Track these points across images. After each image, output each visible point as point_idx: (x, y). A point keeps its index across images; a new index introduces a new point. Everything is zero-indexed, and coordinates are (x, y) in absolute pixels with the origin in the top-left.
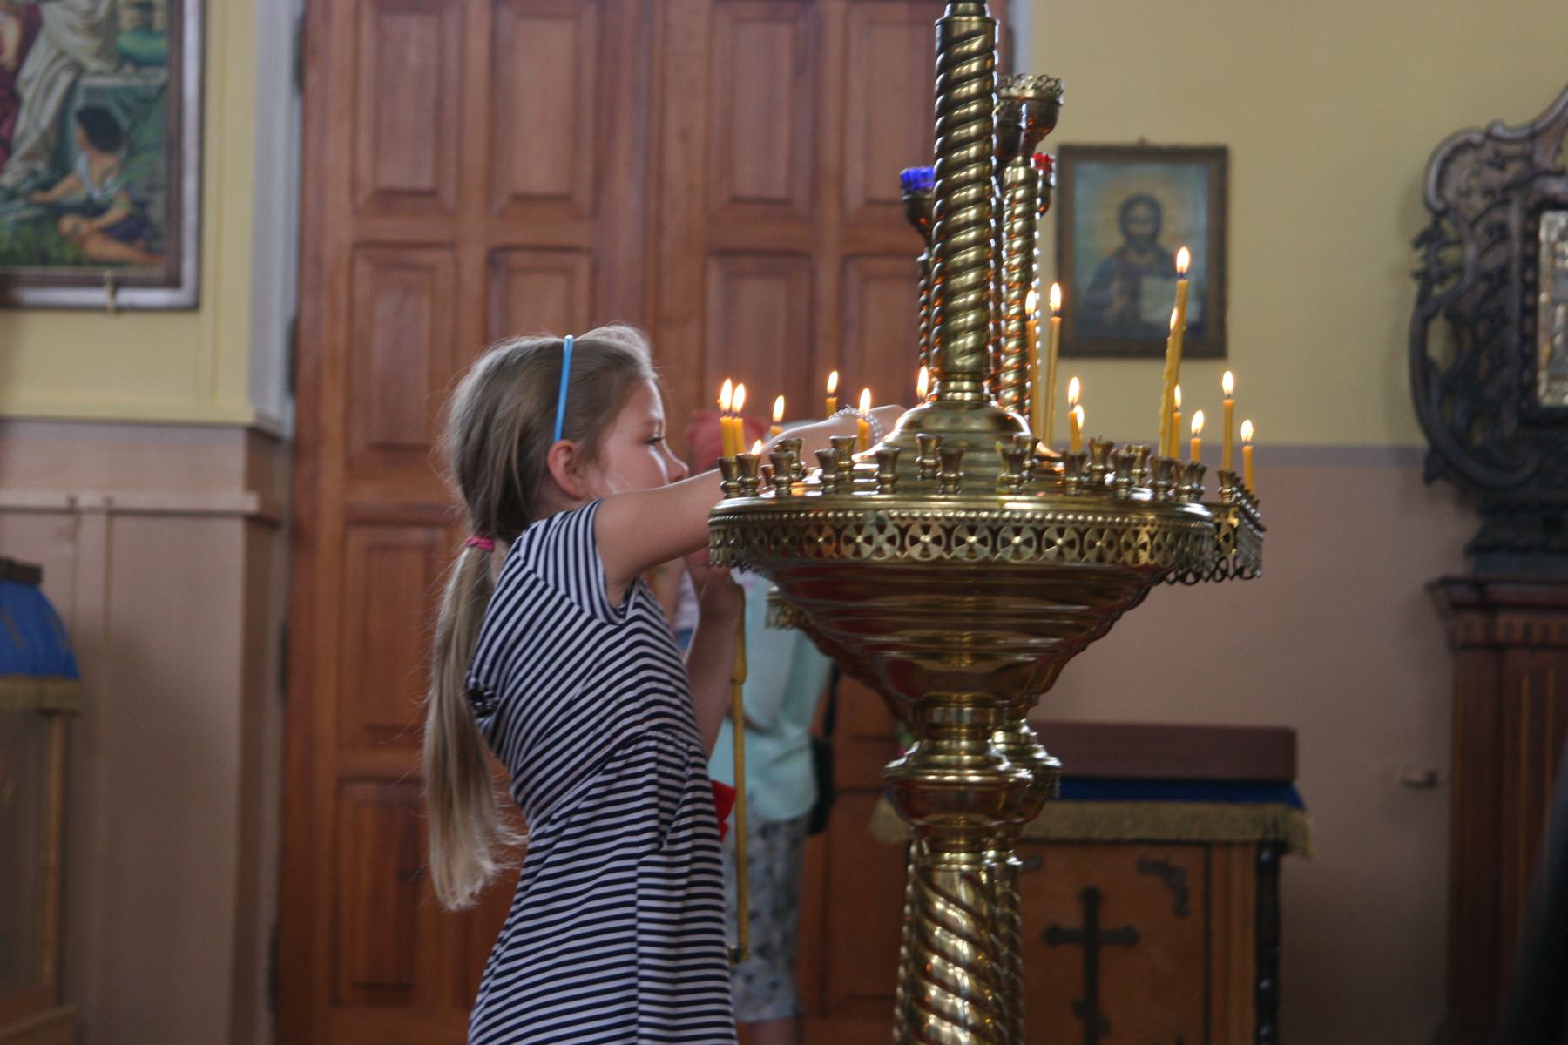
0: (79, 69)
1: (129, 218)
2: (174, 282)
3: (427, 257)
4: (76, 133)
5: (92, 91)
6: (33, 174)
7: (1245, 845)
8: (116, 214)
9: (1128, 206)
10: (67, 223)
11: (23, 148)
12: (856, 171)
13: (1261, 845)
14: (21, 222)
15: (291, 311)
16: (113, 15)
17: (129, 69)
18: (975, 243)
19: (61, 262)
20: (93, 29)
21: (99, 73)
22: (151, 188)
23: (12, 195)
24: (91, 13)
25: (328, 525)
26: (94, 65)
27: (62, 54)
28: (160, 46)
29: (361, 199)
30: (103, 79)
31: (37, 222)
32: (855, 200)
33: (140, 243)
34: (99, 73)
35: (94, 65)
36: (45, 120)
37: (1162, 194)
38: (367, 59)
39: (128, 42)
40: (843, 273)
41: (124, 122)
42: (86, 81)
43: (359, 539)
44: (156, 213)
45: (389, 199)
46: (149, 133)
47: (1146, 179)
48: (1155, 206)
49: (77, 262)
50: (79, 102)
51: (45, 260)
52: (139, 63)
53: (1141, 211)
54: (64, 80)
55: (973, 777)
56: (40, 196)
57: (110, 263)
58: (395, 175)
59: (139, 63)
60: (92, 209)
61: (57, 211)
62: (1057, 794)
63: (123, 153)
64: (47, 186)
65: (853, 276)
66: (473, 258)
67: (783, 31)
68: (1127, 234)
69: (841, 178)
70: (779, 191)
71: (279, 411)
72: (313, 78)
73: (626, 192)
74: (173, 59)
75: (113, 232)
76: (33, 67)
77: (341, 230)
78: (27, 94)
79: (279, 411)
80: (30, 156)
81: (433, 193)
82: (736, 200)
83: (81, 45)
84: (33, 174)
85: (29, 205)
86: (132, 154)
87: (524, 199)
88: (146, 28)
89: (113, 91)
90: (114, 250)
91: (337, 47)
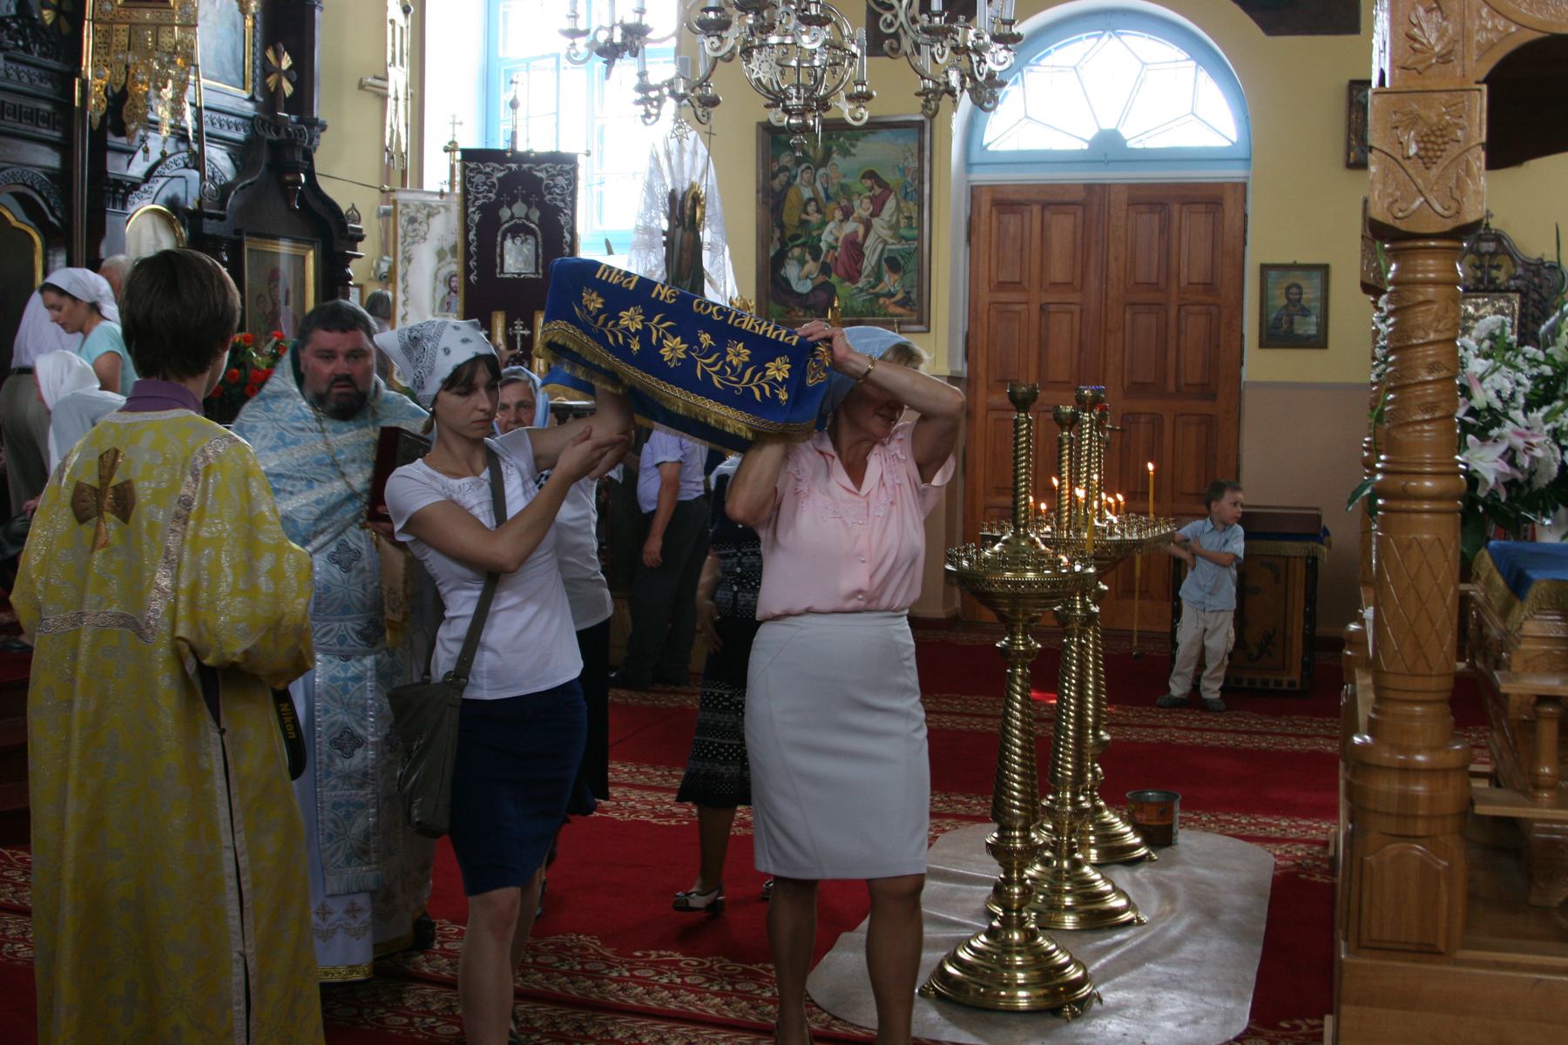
0: (885, 243)
1: (904, 297)
2: (920, 322)
3: (1017, 308)
4: (884, 266)
5: (889, 250)
6: (869, 282)
7: (1302, 557)
8: (899, 296)
9: (1288, 288)
10: (881, 301)
11: (865, 273)
12: (1184, 270)
13: (1307, 557)
14: (865, 300)
15: (966, 329)
16: (898, 221)
17: (904, 241)
18: (1025, 461)
19: (879, 315)
20: (891, 228)
21: (893, 244)
22: (912, 287)
23: (861, 290)
24: (889, 221)
25: (980, 411)
26: (891, 241)
27: (879, 237)
28: (915, 232)
29: (992, 286)
30: (895, 246)
31: (871, 300)
32: (1184, 283)
33: (908, 307)
34: (893, 244)
35: (891, 241)
36: (873, 263)
37: (1303, 283)
38: (994, 231)
39: (903, 232)
40: (1179, 311)
41: (902, 262)
42: (888, 247)
43: (993, 415)
44: (914, 296)
45: (1002, 286)
46: (911, 266)
47: (1296, 276)
48: (1299, 287)
49: (885, 315)
50: (885, 255)
51: (874, 315)
52: (907, 239)
53: (1294, 290)
54: (880, 247)
55: (1022, 648)
56: (871, 291)
57: (897, 315)
58: (1004, 277)
59: (907, 239)
60: (890, 295)
61: (878, 296)
62: (947, 722)
63: (901, 274)
64: (874, 287)
65: (1183, 313)
66: (1035, 308)
67: (1156, 218)
68: (1289, 299)
69: (1178, 275)
70: (1154, 280)
71: (961, 368)
72: (974, 239)
73: (1093, 281)
74: (920, 238)
75: (897, 304)
76: (869, 242)
77: (985, 297)
78: (867, 253)
79: (961, 368)
80: (868, 276)
81: (1020, 283)
82: (1136, 284)
83: (886, 234)
84: (869, 282)
85: (869, 294)
86: (904, 274)
87: (1055, 284)
88: (910, 226)
89: (898, 251)
90: (899, 310)
91: (983, 228)
